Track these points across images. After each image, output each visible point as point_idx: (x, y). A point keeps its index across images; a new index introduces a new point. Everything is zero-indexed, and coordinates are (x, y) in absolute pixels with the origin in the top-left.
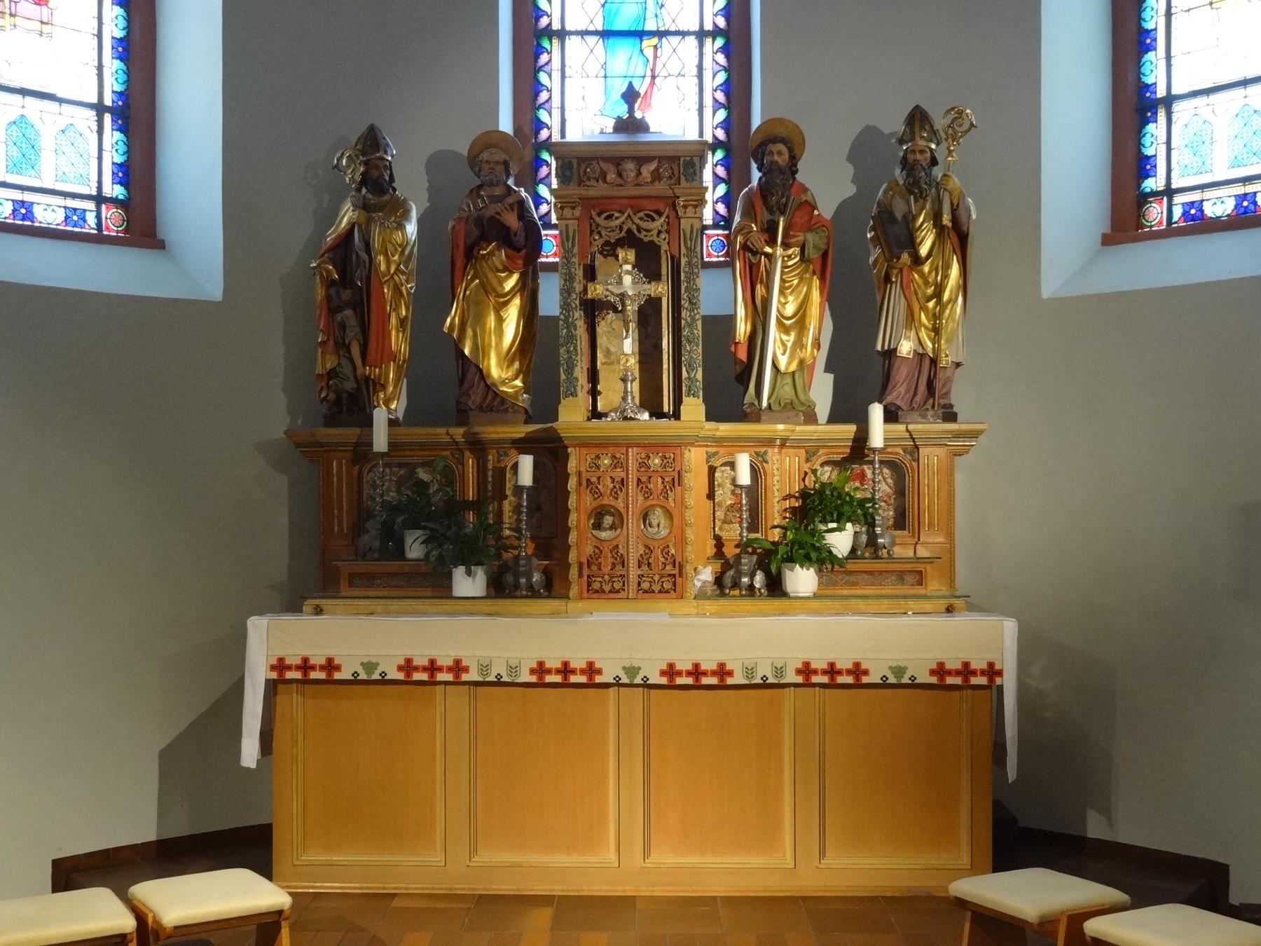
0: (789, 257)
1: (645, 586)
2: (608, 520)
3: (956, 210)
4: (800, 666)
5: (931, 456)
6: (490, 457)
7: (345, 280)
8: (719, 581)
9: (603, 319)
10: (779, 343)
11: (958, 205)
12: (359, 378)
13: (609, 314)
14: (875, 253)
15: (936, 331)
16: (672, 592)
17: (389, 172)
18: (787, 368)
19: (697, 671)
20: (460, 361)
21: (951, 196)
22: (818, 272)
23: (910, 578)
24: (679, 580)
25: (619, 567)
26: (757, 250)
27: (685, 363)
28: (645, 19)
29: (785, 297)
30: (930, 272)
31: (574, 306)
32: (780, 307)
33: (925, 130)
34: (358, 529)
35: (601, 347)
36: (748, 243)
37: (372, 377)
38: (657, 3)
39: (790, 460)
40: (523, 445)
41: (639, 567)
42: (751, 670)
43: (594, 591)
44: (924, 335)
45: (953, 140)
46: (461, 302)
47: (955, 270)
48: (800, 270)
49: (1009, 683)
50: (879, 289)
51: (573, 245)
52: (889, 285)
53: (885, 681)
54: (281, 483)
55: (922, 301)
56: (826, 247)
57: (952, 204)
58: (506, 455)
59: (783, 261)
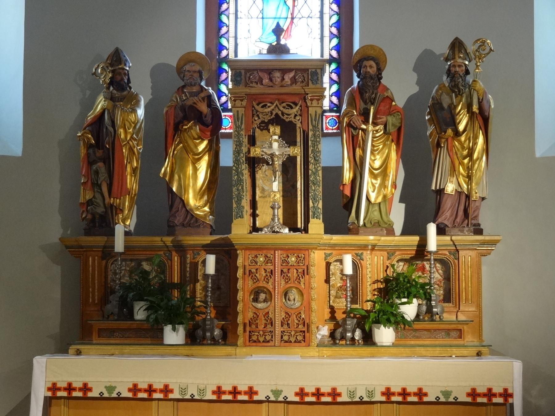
1: (286, 338)
2: (262, 296)
4: (384, 390)
5: (466, 256)
6: (188, 256)
7: (99, 144)
8: (332, 335)
9: (260, 169)
10: (370, 185)
12: (107, 206)
13: (264, 166)
14: (431, 129)
15: (469, 177)
16: (303, 342)
17: (127, 77)
18: (375, 201)
19: (152, 391)
20: (170, 195)
23: (454, 334)
24: (307, 335)
25: (269, 326)
27: (311, 197)
29: (374, 156)
30: (465, 141)
31: (242, 161)
34: (104, 300)
35: (259, 187)
36: (351, 122)
37: (115, 205)
40: (209, 248)
41: (282, 326)
42: (184, 389)
43: (253, 341)
46: (171, 158)
47: (481, 140)
48: (383, 139)
49: (517, 401)
51: (241, 124)
52: (439, 149)
53: (438, 400)
54: (57, 270)
55: (460, 159)
57: (479, 99)
58: (199, 254)
59: (373, 133)
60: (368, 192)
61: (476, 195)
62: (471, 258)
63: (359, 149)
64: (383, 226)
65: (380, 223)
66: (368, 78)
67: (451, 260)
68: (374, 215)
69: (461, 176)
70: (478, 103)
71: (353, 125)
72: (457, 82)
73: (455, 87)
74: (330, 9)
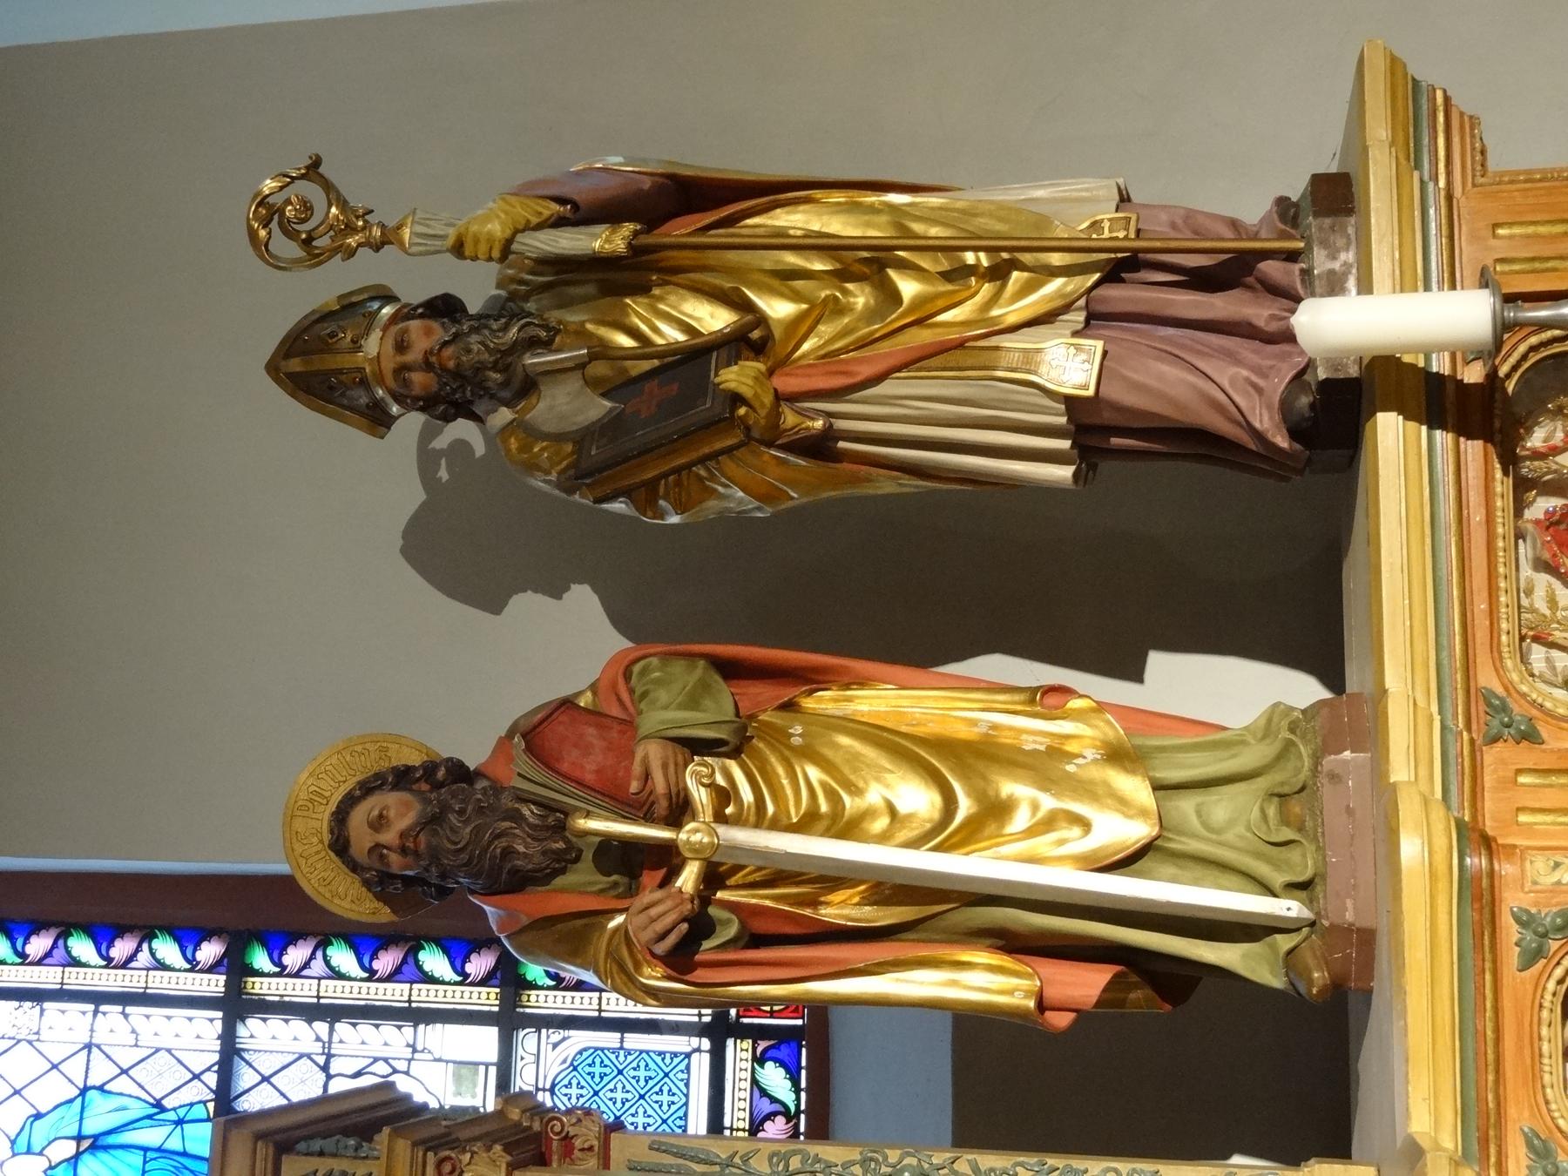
0: (723, 796)
3: (576, 206)
10: (1042, 844)
11: (561, 200)
18: (1143, 813)
21: (529, 228)
22: (786, 693)
26: (684, 920)
28: (184, 1154)
29: (868, 814)
30: (796, 297)
32: (904, 835)
33: (333, 335)
36: (661, 948)
38: (150, 1117)
39: (1534, 810)
44: (1012, 311)
45: (352, 230)
47: (793, 219)
48: (773, 760)
50: (856, 480)
52: (842, 444)
55: (895, 319)
56: (702, 663)
57: (559, 223)
59: (737, 821)
60: (689, 234)
61: (1106, 225)
62: (1511, 224)
63: (827, 904)
64: (1307, 762)
65: (1286, 790)
66: (434, 842)
67: (1522, 348)
68: (1231, 823)
69: (995, 312)
70: (582, 229)
71: (672, 940)
72: (486, 356)
73: (510, 365)
74: (305, 973)
